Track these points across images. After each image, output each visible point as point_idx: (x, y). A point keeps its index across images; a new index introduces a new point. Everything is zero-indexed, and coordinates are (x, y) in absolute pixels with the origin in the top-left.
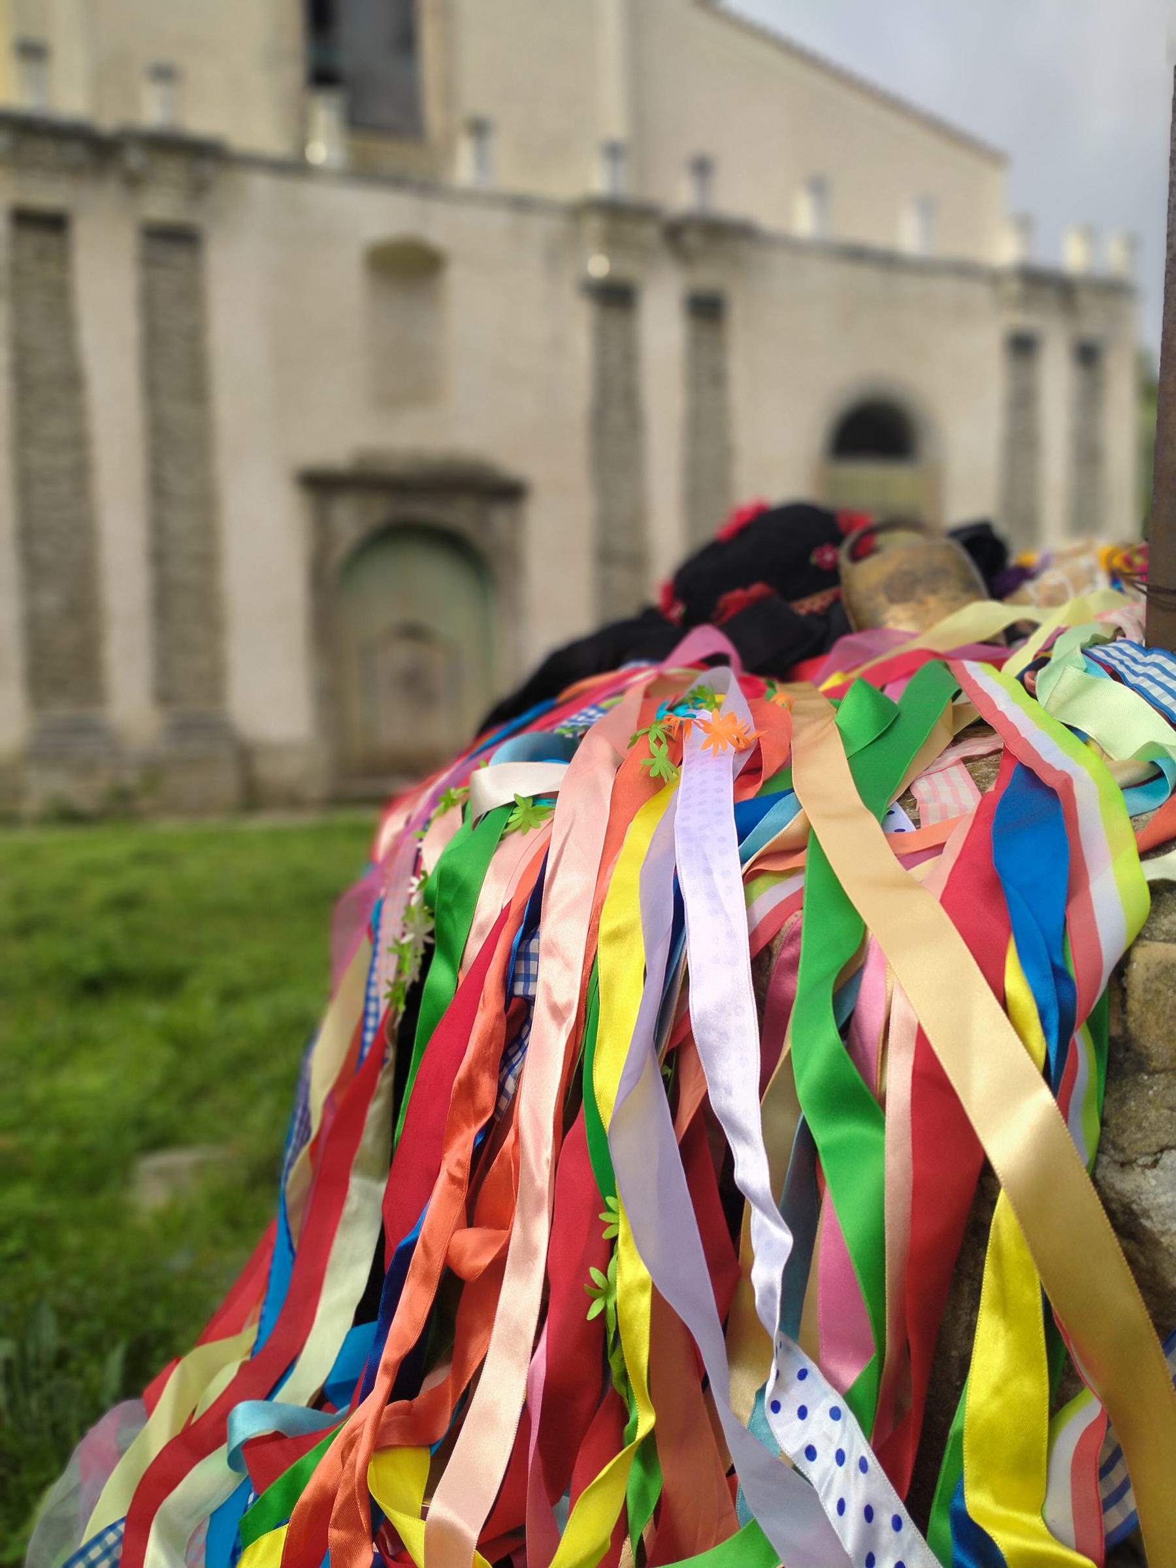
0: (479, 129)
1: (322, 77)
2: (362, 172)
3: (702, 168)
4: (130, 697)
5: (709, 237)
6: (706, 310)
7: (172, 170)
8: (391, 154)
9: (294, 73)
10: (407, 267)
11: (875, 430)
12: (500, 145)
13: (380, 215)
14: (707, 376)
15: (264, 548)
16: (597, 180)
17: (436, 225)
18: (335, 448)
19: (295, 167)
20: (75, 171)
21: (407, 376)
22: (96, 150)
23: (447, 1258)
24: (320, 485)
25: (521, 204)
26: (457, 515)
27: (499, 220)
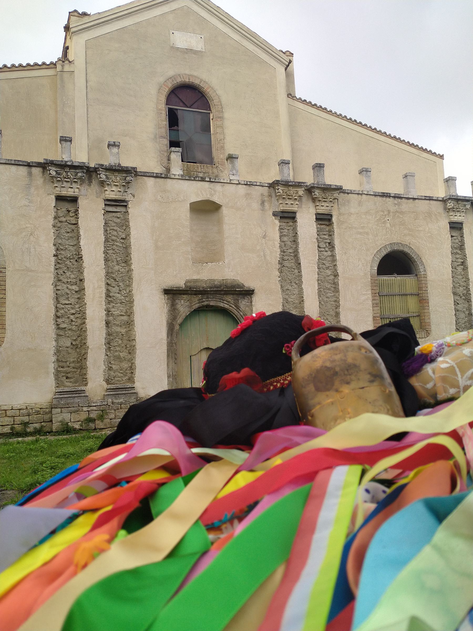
0: (231, 158)
1: (174, 144)
2: (188, 176)
3: (319, 167)
4: (96, 384)
5: (319, 191)
6: (324, 219)
7: (118, 178)
8: (199, 169)
9: (166, 142)
10: (206, 209)
11: (396, 263)
12: (239, 163)
13: (196, 191)
14: (327, 245)
15: (150, 317)
16: (273, 174)
17: (216, 193)
18: (179, 282)
19: (166, 175)
20: (82, 180)
21: (211, 252)
22: (89, 173)
23: (90, 185)
24: (171, 293)
25: (249, 184)
26: (227, 303)
27: (242, 190)
